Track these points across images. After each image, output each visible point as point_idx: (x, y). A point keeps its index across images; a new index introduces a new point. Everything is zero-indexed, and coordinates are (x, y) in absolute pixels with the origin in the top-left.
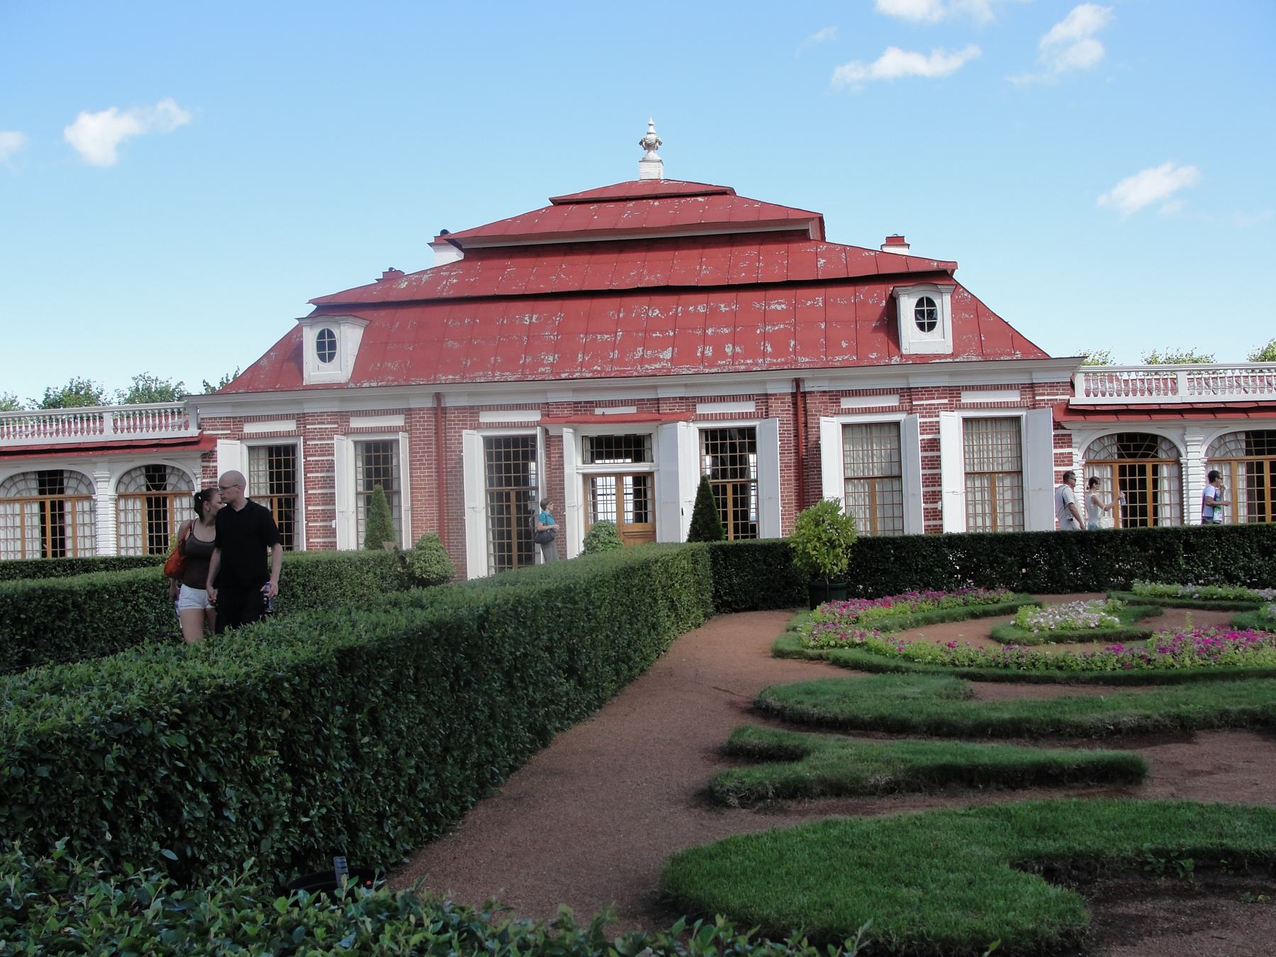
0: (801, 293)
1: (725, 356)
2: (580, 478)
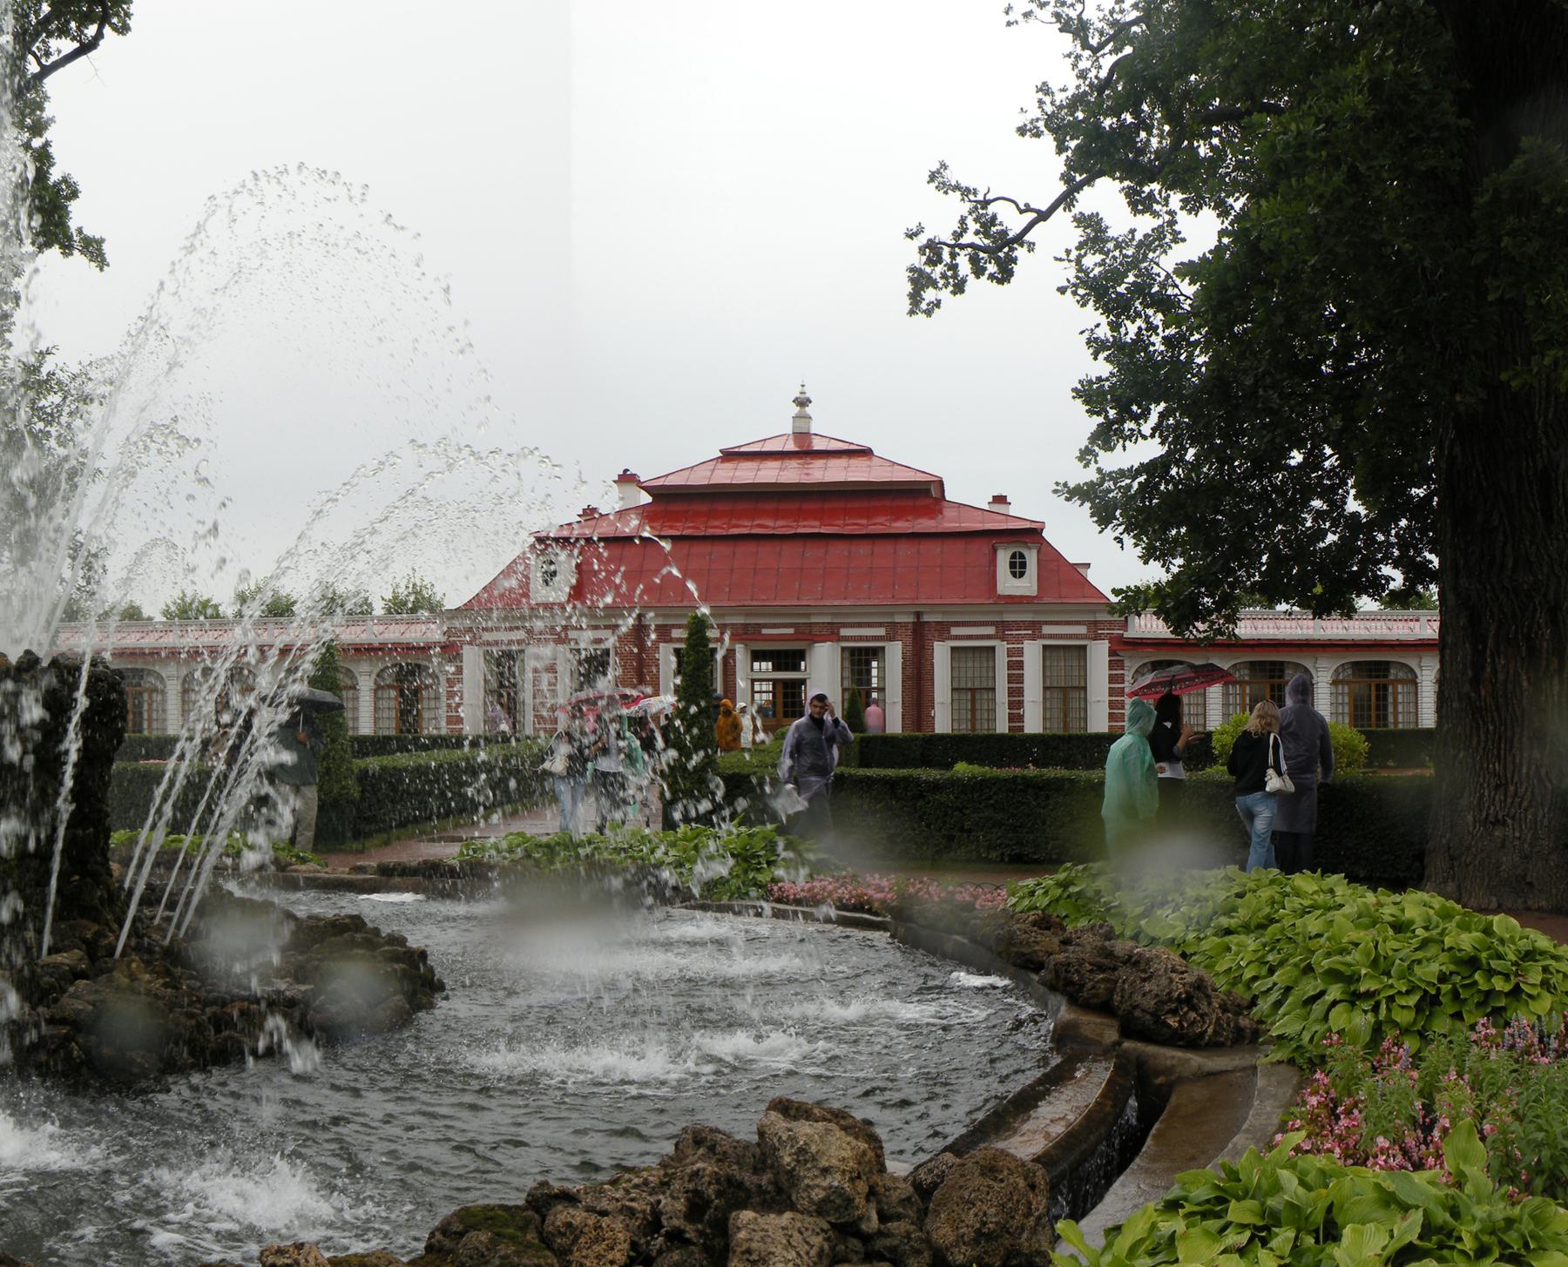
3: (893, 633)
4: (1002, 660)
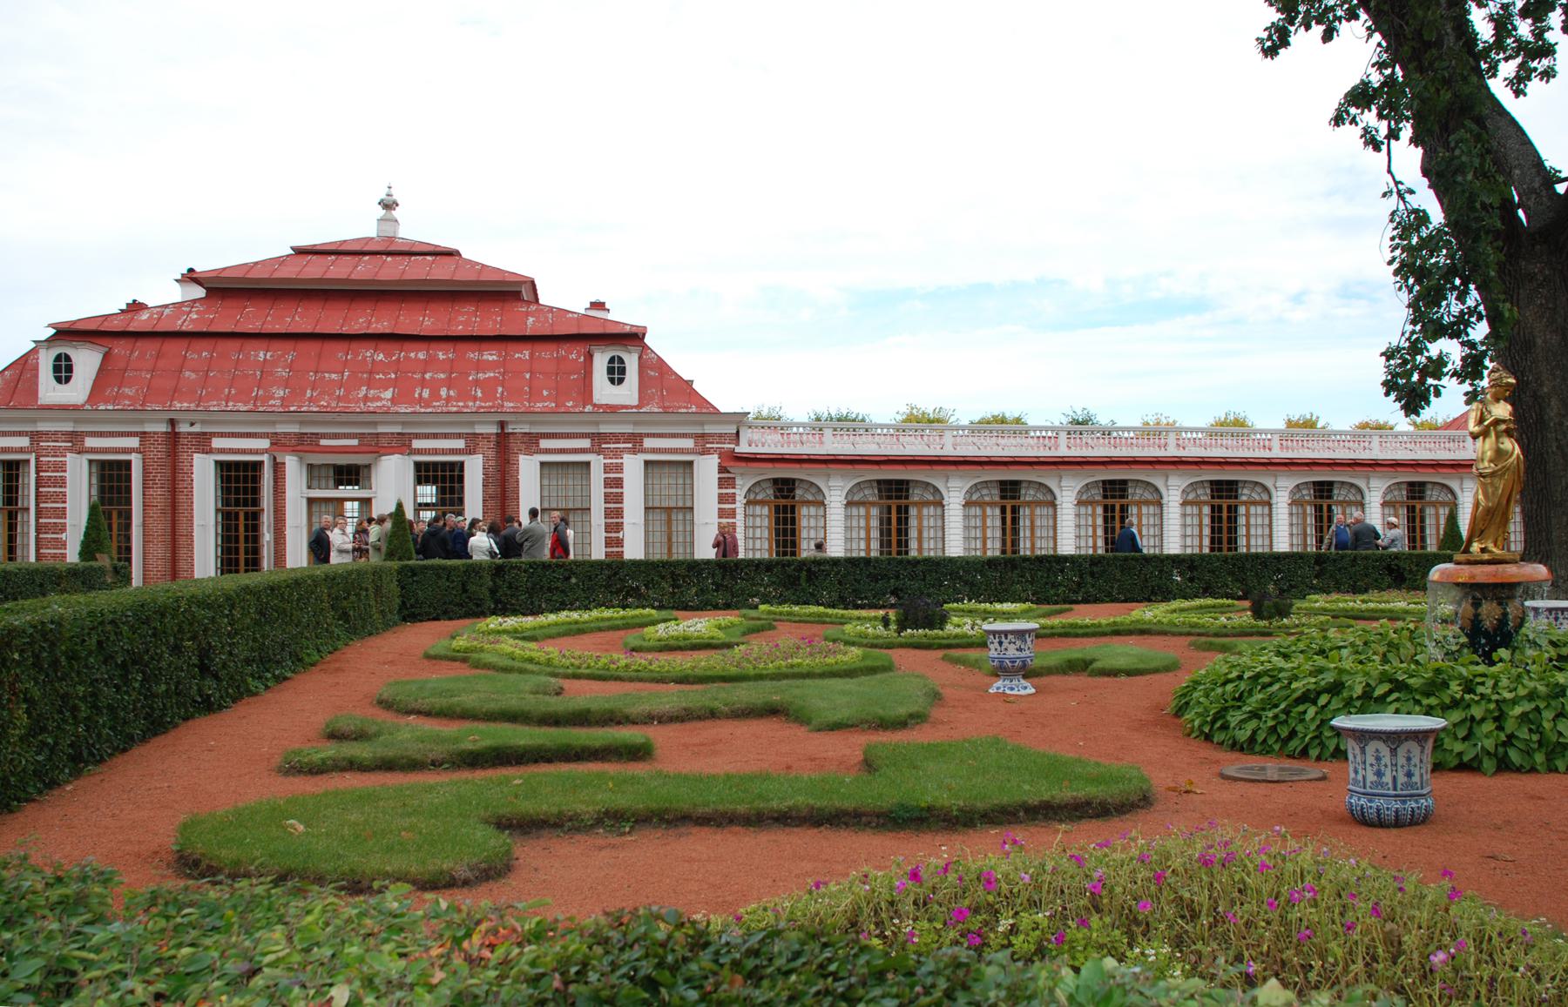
0: (511, 346)
1: (439, 398)
2: (304, 502)
3: (473, 443)
4: (597, 476)
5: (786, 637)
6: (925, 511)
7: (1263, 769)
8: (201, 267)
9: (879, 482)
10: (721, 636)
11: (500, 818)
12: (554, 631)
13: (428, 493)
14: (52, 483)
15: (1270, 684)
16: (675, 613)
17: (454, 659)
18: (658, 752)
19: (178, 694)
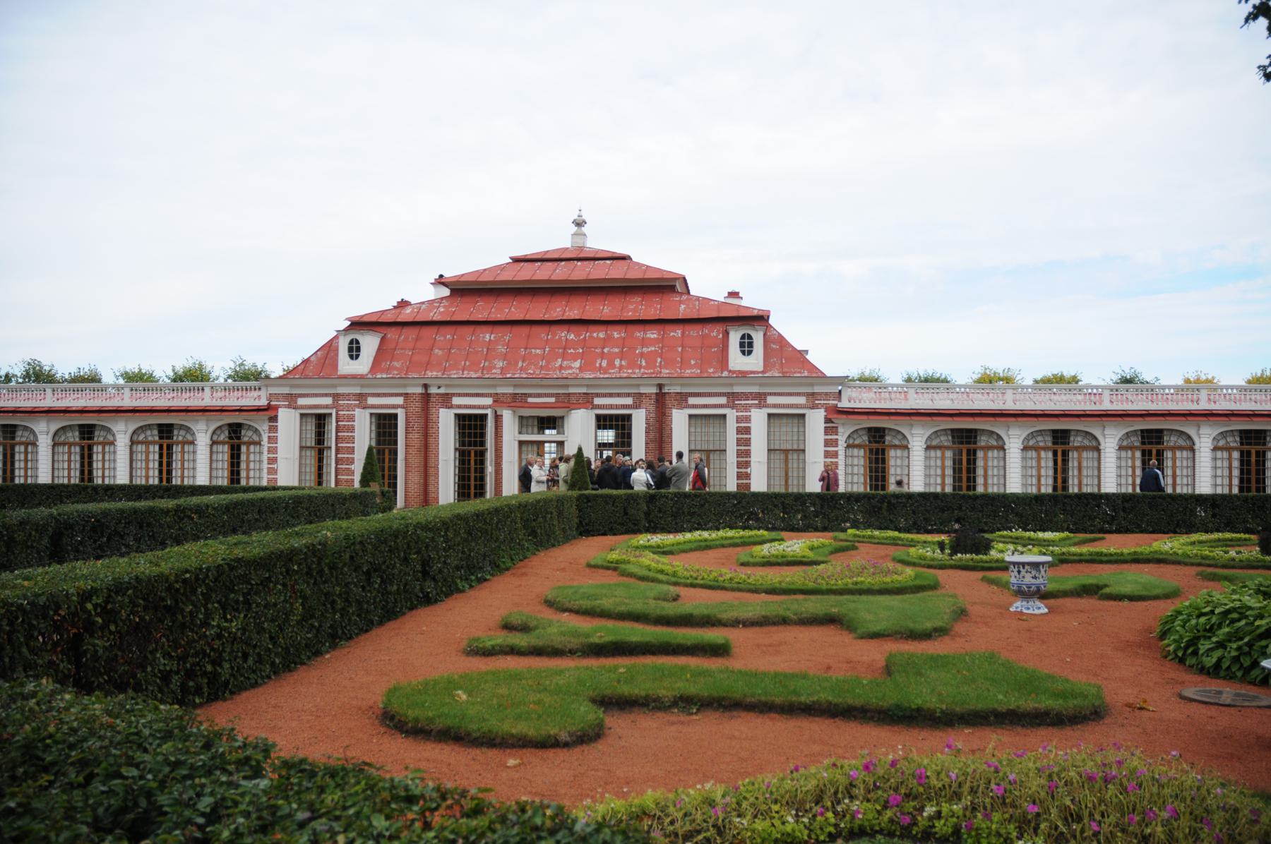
0: (668, 327)
3: (639, 400)
4: (731, 425)
5: (856, 560)
6: (990, 454)
7: (1220, 693)
8: (449, 274)
9: (952, 430)
10: (811, 555)
11: (604, 697)
12: (686, 547)
13: (608, 436)
14: (346, 429)
15: (1239, 620)
16: (784, 534)
17: (608, 568)
18: (734, 650)
19: (405, 592)
